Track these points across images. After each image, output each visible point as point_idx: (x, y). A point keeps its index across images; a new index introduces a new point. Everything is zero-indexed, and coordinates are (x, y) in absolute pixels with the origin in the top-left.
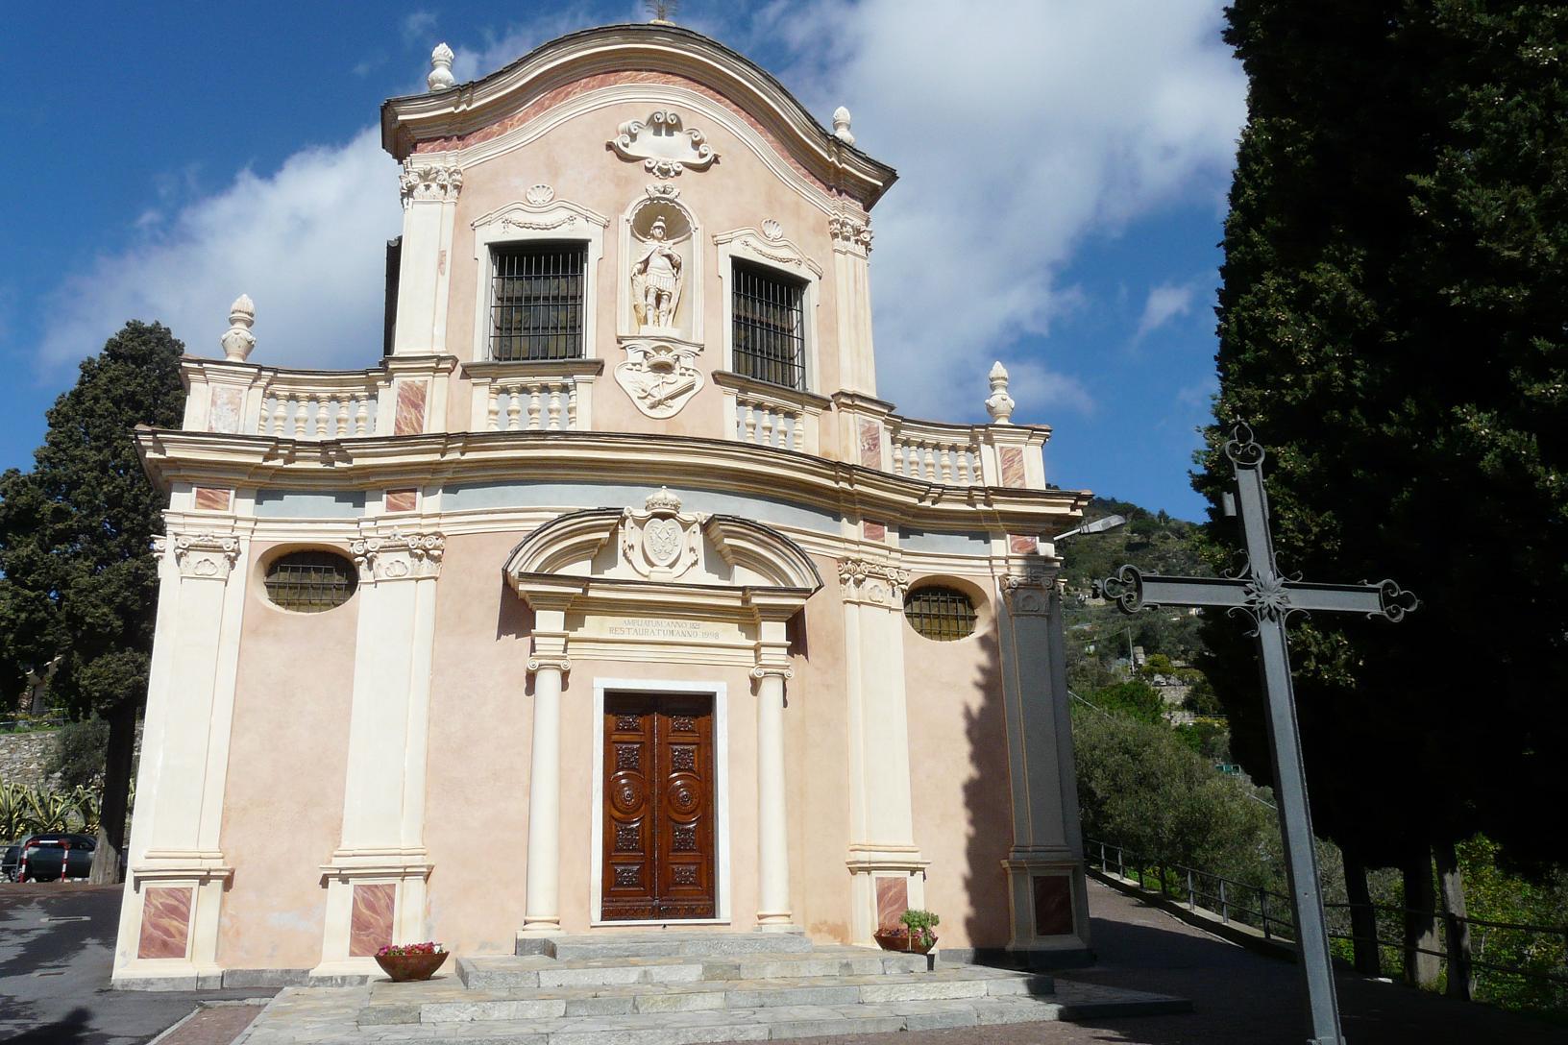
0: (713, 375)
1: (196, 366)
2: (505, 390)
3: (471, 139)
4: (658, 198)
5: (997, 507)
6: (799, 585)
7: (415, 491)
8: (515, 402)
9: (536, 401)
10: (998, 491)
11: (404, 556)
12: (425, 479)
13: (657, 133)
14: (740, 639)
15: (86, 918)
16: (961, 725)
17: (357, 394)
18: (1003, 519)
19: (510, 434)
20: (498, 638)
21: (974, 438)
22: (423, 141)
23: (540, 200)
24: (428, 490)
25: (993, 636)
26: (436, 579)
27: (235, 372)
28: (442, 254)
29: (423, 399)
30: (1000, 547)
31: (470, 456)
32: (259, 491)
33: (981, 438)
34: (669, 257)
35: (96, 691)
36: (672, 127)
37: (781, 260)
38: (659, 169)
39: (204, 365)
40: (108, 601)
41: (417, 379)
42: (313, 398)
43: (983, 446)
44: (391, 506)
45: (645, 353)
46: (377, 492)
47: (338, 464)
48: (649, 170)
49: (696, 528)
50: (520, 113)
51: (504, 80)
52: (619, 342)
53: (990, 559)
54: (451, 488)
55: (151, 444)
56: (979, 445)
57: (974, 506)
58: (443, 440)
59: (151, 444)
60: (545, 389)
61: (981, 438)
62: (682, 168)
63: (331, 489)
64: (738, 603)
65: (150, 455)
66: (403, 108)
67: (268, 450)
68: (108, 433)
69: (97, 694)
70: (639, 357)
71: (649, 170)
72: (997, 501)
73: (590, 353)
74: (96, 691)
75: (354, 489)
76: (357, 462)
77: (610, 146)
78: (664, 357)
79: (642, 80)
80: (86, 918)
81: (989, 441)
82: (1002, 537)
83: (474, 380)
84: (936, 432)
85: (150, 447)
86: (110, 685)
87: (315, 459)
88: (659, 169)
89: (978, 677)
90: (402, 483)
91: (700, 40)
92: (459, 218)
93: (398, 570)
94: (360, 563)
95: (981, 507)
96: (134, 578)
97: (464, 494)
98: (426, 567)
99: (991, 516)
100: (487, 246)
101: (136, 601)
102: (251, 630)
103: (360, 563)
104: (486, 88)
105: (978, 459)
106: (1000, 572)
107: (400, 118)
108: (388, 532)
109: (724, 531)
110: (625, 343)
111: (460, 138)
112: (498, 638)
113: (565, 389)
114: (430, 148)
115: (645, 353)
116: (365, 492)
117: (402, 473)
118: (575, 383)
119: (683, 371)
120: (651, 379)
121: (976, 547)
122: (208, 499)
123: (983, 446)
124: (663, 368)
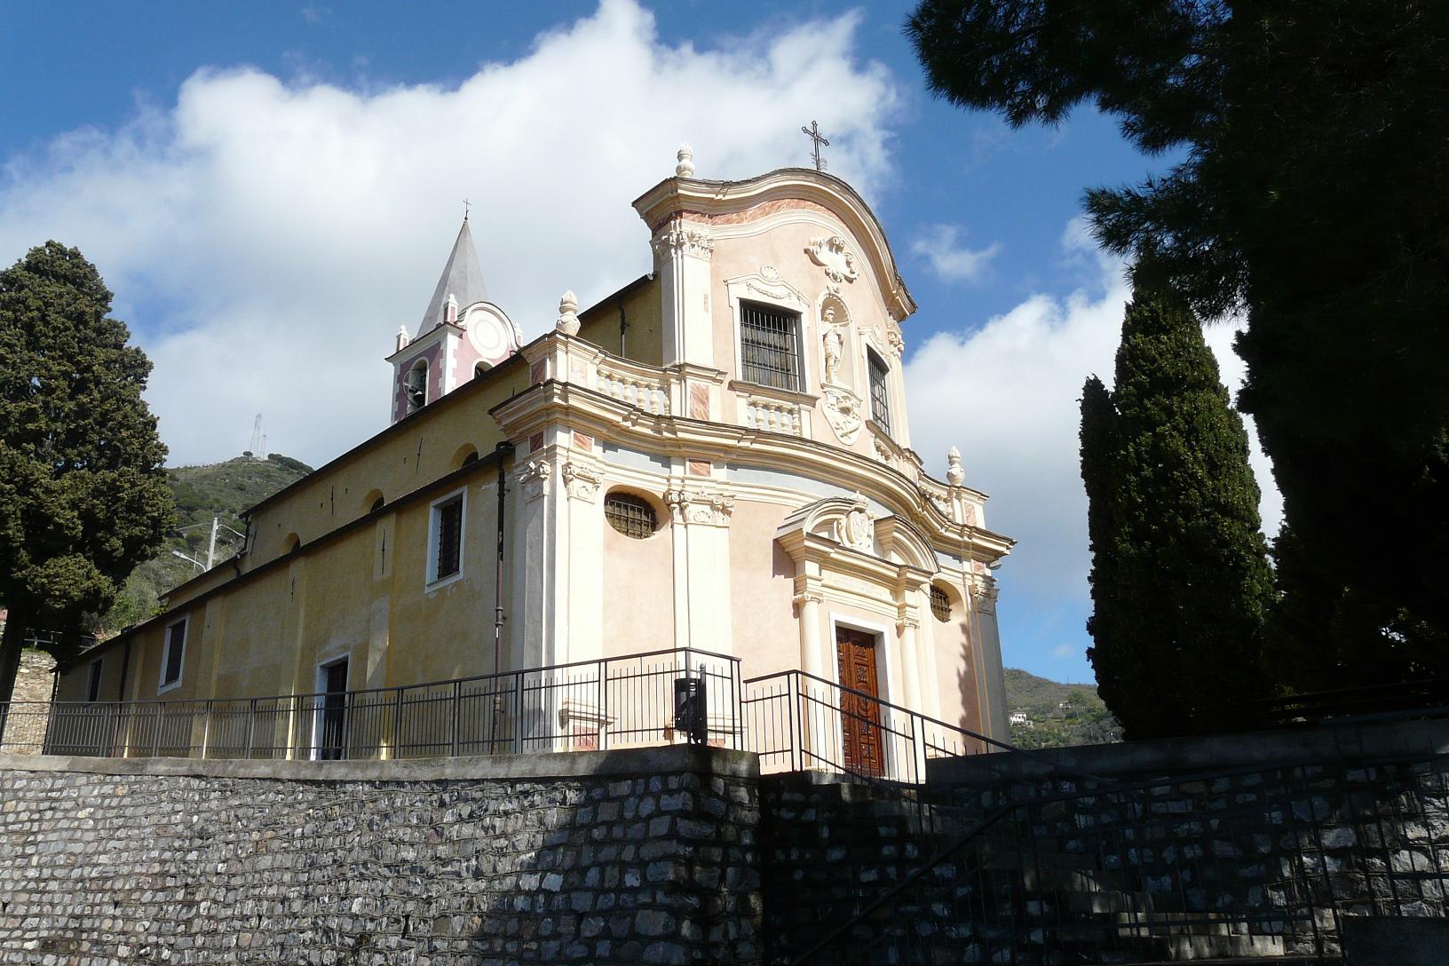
0: (866, 422)
1: (563, 338)
2: (754, 404)
3: (717, 219)
4: (833, 295)
5: (975, 540)
6: (925, 568)
7: (709, 463)
8: (761, 413)
9: (774, 416)
10: (978, 531)
11: (707, 508)
12: (719, 456)
13: (831, 250)
14: (890, 599)
15: (1396, 636)
16: (956, 681)
17: (652, 384)
18: (973, 549)
19: (786, 436)
20: (774, 576)
21: (949, 493)
22: (690, 212)
23: (770, 277)
24: (719, 465)
25: (966, 624)
26: (728, 527)
27: (585, 349)
28: (706, 297)
29: (707, 398)
30: (967, 566)
31: (756, 446)
32: (604, 442)
33: (954, 494)
34: (839, 335)
35: (57, 590)
36: (839, 249)
37: (881, 353)
38: (833, 275)
39: (570, 339)
40: (74, 505)
41: (703, 383)
42: (622, 381)
43: (954, 499)
44: (694, 471)
45: (838, 398)
46: (682, 460)
47: (665, 434)
48: (828, 274)
49: (872, 520)
50: (751, 211)
51: (750, 186)
52: (822, 388)
53: (963, 574)
54: (733, 466)
55: (559, 392)
56: (952, 498)
57: (962, 537)
58: (743, 432)
59: (559, 392)
60: (779, 409)
61: (954, 494)
62: (843, 278)
63: (647, 450)
64: (895, 576)
65: (556, 400)
66: (683, 185)
67: (627, 413)
68: (66, 346)
69: (57, 593)
70: (834, 401)
71: (828, 274)
72: (975, 537)
73: (809, 392)
74: (57, 590)
75: (665, 454)
76: (680, 435)
77: (806, 251)
78: (847, 404)
79: (817, 210)
80: (1396, 636)
81: (959, 498)
82: (969, 561)
83: (738, 393)
84: (929, 483)
85: (557, 394)
86: (70, 585)
87: (648, 427)
88: (833, 275)
89: (962, 650)
90: (703, 455)
91: (854, 194)
92: (715, 274)
93: (703, 518)
94: (675, 508)
95: (966, 539)
96: (109, 488)
97: (742, 472)
98: (719, 518)
99: (967, 545)
100: (738, 300)
101: (102, 510)
102: (608, 547)
103: (675, 508)
104: (738, 189)
105: (950, 507)
106: (969, 583)
107: (679, 191)
108: (696, 490)
109: (897, 527)
110: (826, 389)
111: (711, 217)
112: (774, 576)
113: (791, 412)
114: (691, 218)
115: (838, 398)
116: (669, 457)
117: (705, 449)
118: (800, 409)
119: (854, 415)
120: (840, 417)
121: (954, 564)
122: (580, 441)
123: (954, 499)
124: (846, 411)
